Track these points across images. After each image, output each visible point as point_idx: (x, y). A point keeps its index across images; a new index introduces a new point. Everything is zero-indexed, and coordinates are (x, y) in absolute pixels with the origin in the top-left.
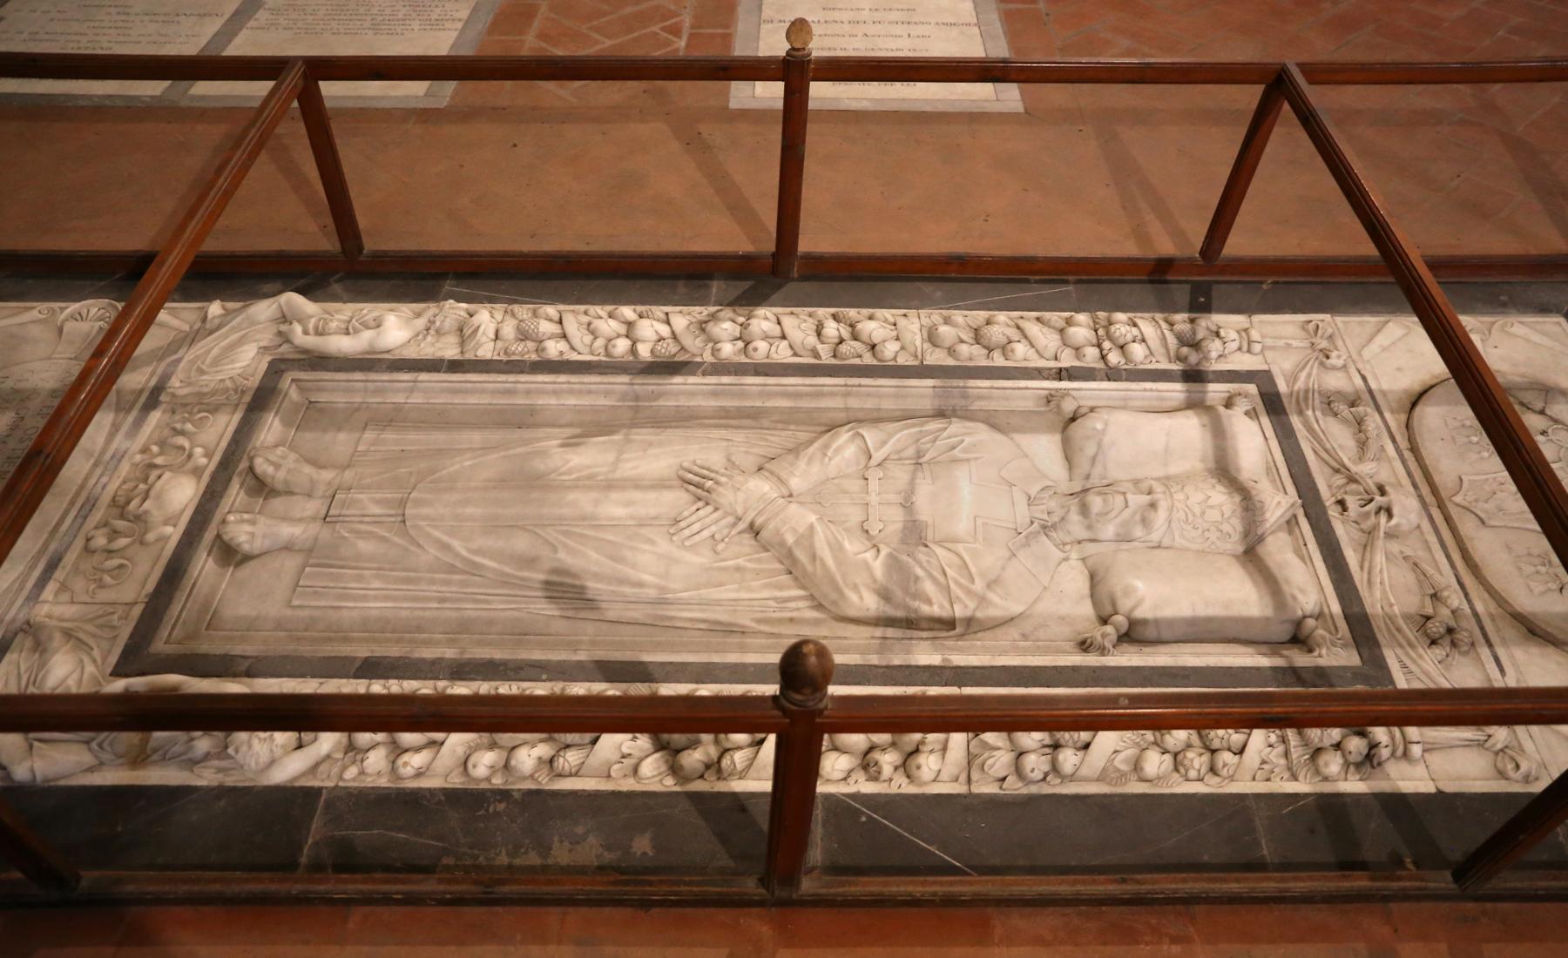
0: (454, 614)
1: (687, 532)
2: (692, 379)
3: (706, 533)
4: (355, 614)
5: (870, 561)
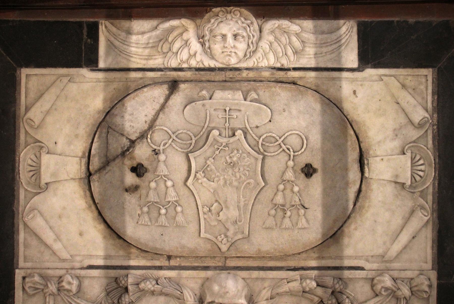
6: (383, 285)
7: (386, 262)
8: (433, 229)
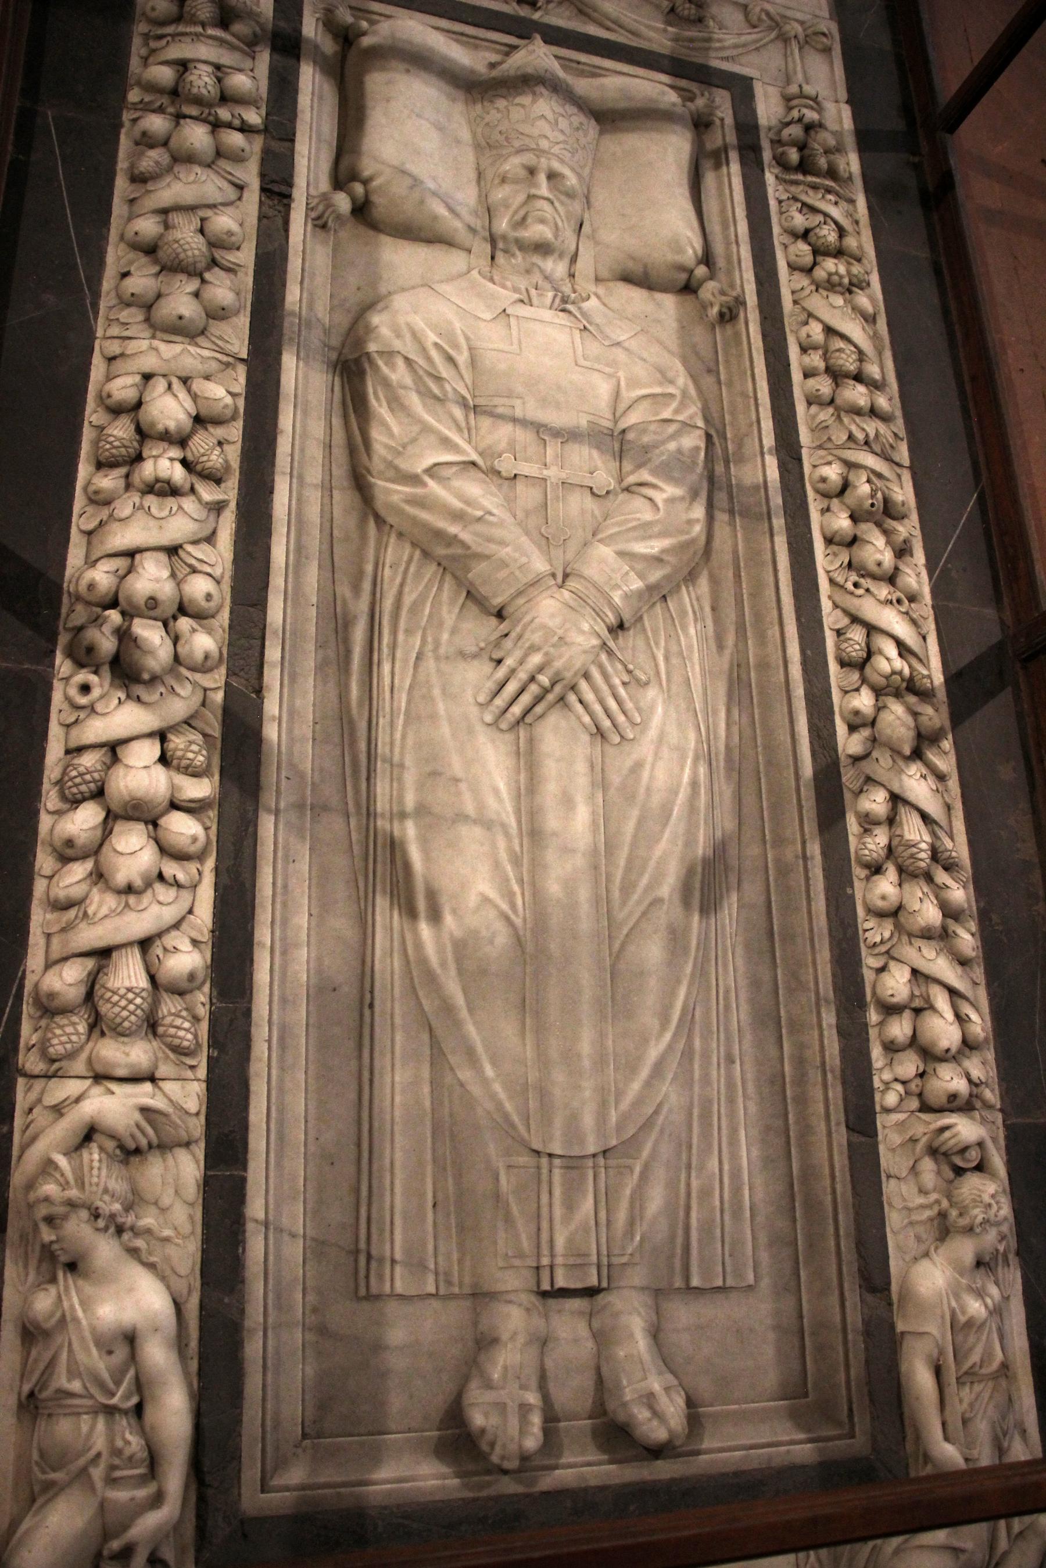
0: (748, 1037)
1: (621, 719)
2: (271, 706)
3: (622, 691)
4: (758, 1181)
5: (665, 496)
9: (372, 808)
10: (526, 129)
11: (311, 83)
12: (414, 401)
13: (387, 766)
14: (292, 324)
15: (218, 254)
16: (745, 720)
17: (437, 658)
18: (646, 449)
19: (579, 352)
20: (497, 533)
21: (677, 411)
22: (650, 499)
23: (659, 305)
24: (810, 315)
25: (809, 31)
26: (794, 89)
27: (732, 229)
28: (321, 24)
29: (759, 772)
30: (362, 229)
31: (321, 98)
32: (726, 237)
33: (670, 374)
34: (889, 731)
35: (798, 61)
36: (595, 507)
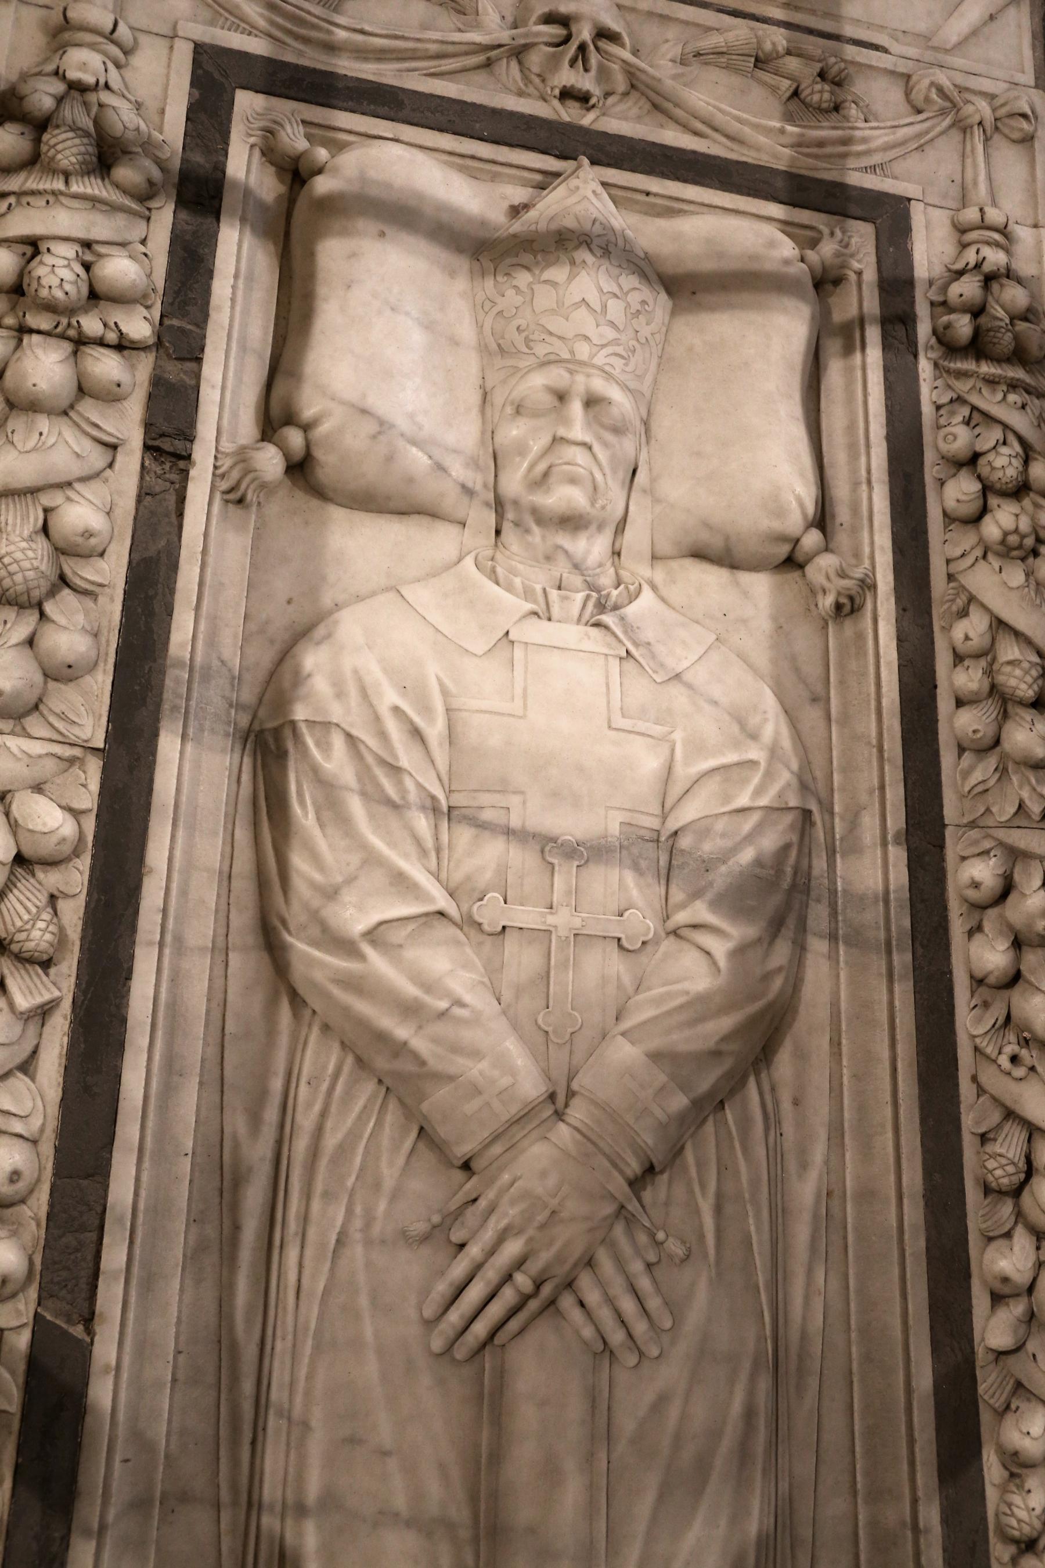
1: (640, 1328)
2: (106, 1349)
3: (644, 1283)
6: (933, 78)
7: (935, 49)
8: (1031, 13)
9: (255, 1497)
10: (556, 324)
11: (237, 253)
12: (356, 807)
13: (284, 1422)
14: (177, 681)
15: (69, 566)
16: (835, 1284)
17: (368, 1243)
18: (707, 866)
19: (616, 703)
20: (468, 1036)
21: (758, 792)
22: (708, 953)
23: (745, 594)
24: (972, 599)
25: (1002, 112)
26: (971, 215)
27: (863, 459)
28: (257, 153)
29: (851, 1373)
30: (302, 500)
31: (250, 278)
32: (854, 471)
33: (754, 721)
34: (969, 361)
35: (982, 165)
36: (622, 968)
